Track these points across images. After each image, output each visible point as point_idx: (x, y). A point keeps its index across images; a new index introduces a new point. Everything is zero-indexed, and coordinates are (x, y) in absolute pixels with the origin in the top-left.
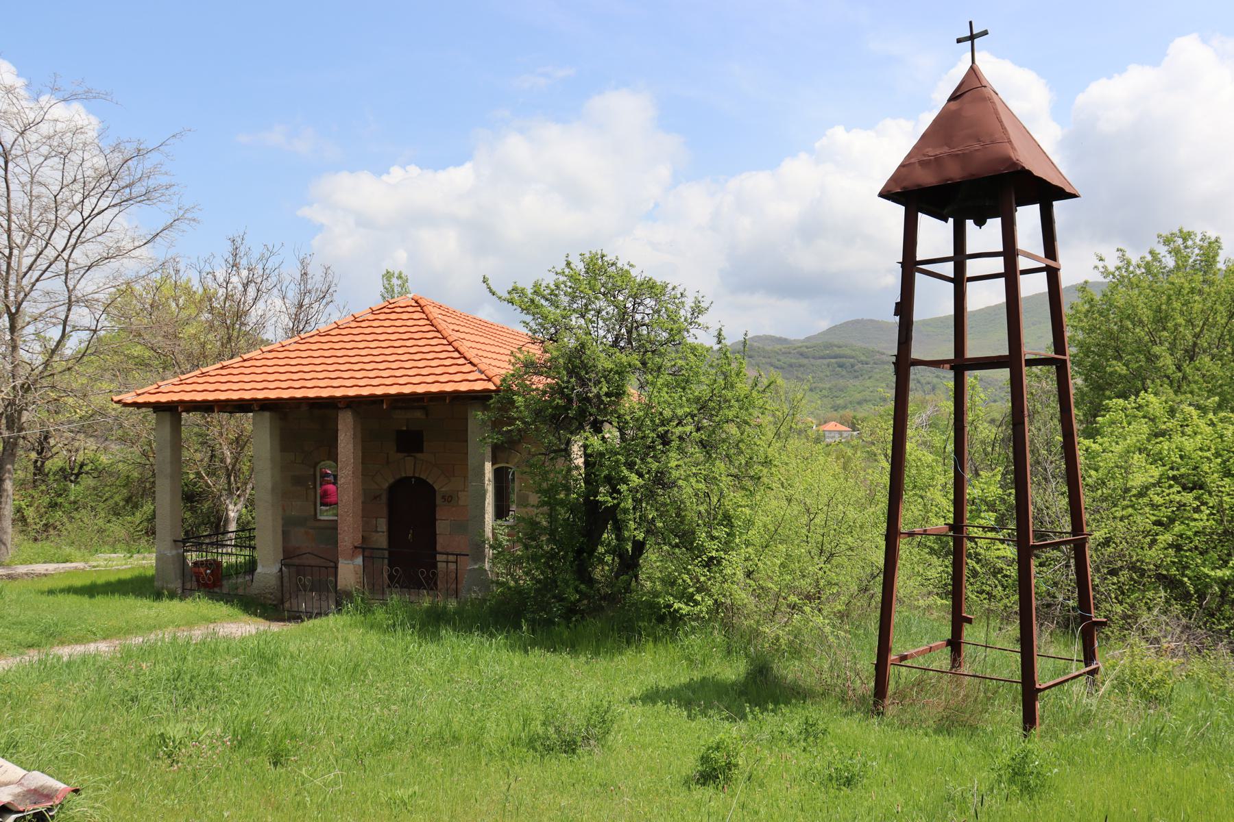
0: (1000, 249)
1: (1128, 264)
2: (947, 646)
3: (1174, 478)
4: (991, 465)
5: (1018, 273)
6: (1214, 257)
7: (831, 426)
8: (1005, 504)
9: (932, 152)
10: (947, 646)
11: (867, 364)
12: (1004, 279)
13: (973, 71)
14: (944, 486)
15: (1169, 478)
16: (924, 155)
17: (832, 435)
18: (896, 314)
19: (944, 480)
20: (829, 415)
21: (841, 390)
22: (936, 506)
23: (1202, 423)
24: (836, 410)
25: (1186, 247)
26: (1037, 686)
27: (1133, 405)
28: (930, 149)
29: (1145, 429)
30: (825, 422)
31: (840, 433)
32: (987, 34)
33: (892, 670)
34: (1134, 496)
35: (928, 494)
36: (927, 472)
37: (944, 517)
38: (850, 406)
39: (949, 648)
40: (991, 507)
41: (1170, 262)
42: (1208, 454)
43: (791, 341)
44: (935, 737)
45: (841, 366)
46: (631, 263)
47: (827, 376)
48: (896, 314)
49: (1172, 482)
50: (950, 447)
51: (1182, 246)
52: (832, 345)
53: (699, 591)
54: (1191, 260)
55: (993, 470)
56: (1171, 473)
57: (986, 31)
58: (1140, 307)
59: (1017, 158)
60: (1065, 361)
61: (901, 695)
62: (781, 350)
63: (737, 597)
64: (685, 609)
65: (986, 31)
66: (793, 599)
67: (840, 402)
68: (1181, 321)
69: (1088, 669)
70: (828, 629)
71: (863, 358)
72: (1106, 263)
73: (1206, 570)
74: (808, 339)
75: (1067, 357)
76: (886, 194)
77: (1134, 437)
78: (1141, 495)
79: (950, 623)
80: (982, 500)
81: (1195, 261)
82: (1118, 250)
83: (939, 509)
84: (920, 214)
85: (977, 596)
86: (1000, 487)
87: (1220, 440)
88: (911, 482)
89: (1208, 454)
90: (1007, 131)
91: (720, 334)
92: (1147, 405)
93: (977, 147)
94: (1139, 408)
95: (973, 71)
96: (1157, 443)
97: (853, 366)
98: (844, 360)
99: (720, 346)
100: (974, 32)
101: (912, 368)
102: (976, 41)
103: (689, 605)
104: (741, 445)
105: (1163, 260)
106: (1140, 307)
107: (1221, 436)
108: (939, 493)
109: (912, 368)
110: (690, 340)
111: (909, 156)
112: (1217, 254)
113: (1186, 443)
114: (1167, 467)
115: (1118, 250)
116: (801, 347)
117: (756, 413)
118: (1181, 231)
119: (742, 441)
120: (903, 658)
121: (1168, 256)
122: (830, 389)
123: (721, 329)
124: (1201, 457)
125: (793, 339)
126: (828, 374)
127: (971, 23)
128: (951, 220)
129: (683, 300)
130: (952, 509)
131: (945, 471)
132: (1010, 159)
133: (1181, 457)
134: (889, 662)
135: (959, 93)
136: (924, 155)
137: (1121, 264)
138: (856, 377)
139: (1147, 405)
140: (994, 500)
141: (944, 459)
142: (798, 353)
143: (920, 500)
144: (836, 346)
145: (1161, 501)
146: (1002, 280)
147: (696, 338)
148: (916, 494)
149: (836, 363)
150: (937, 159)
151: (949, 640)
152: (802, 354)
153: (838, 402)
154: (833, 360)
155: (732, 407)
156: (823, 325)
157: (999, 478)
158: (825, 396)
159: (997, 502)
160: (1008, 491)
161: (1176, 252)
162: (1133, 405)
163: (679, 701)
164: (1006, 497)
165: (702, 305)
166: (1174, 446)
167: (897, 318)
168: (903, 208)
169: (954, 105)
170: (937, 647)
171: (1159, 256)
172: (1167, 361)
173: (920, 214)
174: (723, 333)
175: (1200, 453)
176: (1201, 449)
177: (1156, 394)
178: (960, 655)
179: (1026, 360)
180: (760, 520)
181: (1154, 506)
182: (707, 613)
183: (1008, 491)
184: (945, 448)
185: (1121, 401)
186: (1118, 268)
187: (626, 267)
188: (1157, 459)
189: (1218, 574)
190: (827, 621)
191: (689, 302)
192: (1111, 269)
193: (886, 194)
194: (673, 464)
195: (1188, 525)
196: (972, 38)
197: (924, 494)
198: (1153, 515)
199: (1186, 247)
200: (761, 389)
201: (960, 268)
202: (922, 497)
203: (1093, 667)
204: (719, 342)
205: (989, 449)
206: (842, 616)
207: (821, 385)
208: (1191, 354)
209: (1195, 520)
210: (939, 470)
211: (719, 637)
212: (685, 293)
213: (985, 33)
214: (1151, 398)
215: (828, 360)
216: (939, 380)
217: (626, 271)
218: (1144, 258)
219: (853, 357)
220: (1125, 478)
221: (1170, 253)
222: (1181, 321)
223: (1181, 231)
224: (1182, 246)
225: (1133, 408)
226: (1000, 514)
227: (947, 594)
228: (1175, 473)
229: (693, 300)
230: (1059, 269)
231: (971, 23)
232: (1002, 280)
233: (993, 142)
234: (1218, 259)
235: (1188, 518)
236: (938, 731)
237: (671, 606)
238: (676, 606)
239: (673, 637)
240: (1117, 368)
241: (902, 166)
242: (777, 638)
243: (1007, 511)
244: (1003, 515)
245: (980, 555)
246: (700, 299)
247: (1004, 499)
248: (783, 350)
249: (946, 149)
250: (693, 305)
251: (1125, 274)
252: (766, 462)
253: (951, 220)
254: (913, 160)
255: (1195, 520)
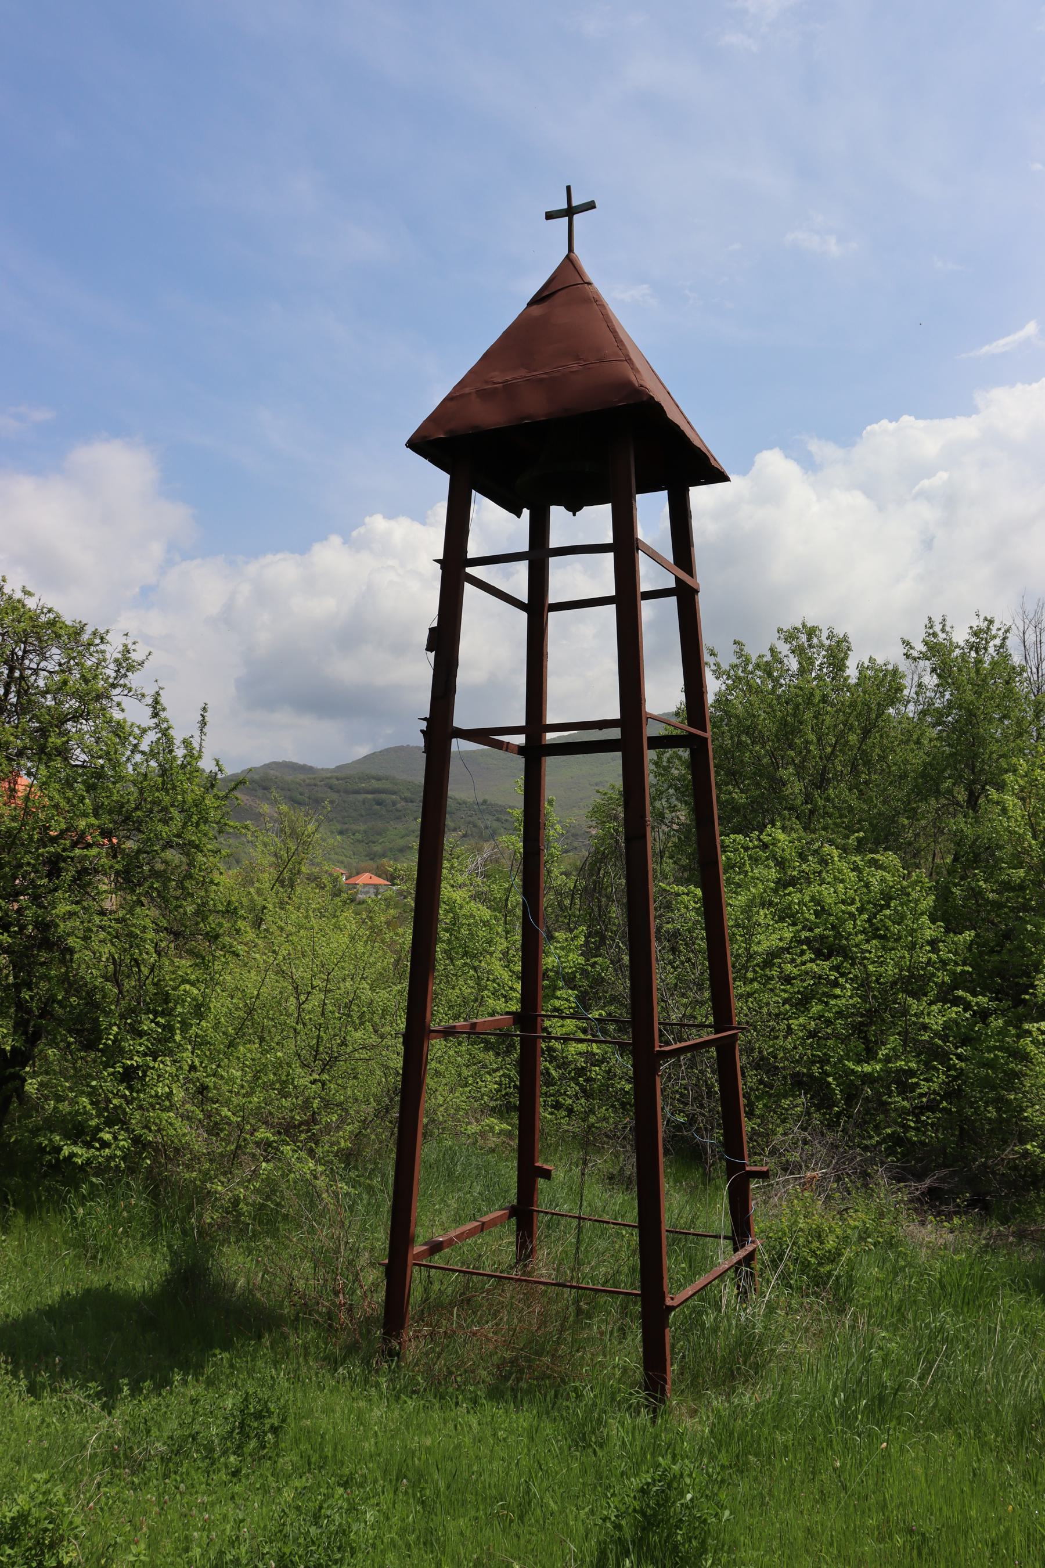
0: (609, 538)
1: (747, 661)
2: (510, 1217)
3: (807, 941)
4: (568, 924)
5: (639, 596)
6: (843, 660)
7: (365, 878)
8: (587, 978)
9: (499, 377)
10: (510, 1217)
11: (412, 802)
12: (614, 606)
13: (570, 261)
14: (505, 953)
15: (801, 942)
16: (487, 382)
17: (366, 889)
18: (429, 648)
19: (505, 944)
20: (363, 864)
21: (379, 834)
22: (494, 981)
23: (844, 866)
24: (372, 859)
25: (811, 646)
26: (669, 1302)
27: (756, 843)
28: (496, 373)
29: (773, 873)
30: (358, 874)
31: (376, 887)
32: (594, 207)
33: (416, 1276)
34: (757, 965)
35: (483, 964)
36: (482, 933)
37: (505, 997)
38: (389, 853)
39: (514, 1220)
40: (570, 982)
41: (793, 664)
42: (852, 909)
43: (318, 770)
44: (489, 1408)
45: (379, 803)
46: (28, 589)
47: (362, 816)
48: (429, 648)
49: (805, 947)
50: (517, 898)
51: (806, 644)
52: (370, 777)
53: (109, 1123)
54: (817, 663)
55: (571, 931)
56: (804, 934)
57: (593, 202)
58: (761, 718)
59: (642, 382)
60: (706, 739)
61: (434, 1307)
62: (304, 781)
63: (172, 1132)
64: (81, 1153)
65: (593, 202)
66: (264, 1133)
67: (377, 848)
68: (812, 737)
69: (742, 1254)
70: (321, 1183)
71: (408, 795)
72: (719, 659)
73: (850, 1065)
74: (339, 768)
75: (708, 735)
76: (420, 444)
77: (760, 885)
78: (768, 964)
79: (515, 1155)
80: (557, 973)
81: (822, 664)
82: (735, 643)
83: (499, 985)
84: (473, 492)
85: (551, 1113)
86: (581, 955)
87: (865, 890)
88: (460, 946)
89: (852, 909)
90: (623, 345)
91: (156, 702)
92: (773, 844)
93: (575, 367)
94: (765, 846)
95: (570, 261)
96: (785, 895)
97: (394, 803)
98: (383, 796)
99: (156, 720)
100: (575, 203)
101: (454, 740)
102: (576, 218)
103: (93, 1147)
104: (187, 884)
105: (785, 660)
106: (761, 718)
107: (867, 885)
108: (497, 963)
109: (454, 740)
110: (117, 715)
111: (461, 384)
112: (846, 657)
113: (825, 893)
114: (799, 927)
115: (735, 643)
116: (329, 778)
117: (211, 830)
118: (804, 625)
119: (189, 876)
120: (435, 1248)
121: (791, 656)
122: (365, 832)
123: (158, 694)
124: (843, 912)
125: (320, 767)
126: (364, 813)
127: (569, 188)
128: (526, 513)
129: (102, 647)
130: (518, 986)
131: (507, 932)
132: (629, 383)
133: (817, 914)
134: (410, 1261)
135: (546, 293)
136: (487, 382)
137: (737, 661)
138: (398, 818)
139: (773, 844)
140: (574, 973)
141: (506, 916)
142: (326, 785)
143: (472, 972)
144: (374, 778)
145: (796, 971)
146: (612, 608)
147: (123, 710)
148: (465, 964)
149: (374, 799)
150: (508, 388)
151: (513, 1207)
152: (331, 788)
153: (375, 849)
154: (370, 796)
155: (171, 819)
156: (362, 751)
157: (582, 940)
158: (359, 841)
159: (577, 975)
160: (593, 960)
161: (799, 651)
162: (756, 843)
163: (13, 1356)
164: (590, 968)
165: (133, 656)
166: (807, 898)
167: (432, 655)
168: (448, 476)
169: (537, 310)
170: (494, 1222)
171: (781, 656)
172: (795, 788)
173: (473, 492)
174: (163, 700)
175: (843, 907)
176: (843, 902)
177: (784, 828)
178: (531, 1235)
179: (649, 739)
180: (219, 1004)
181: (788, 980)
182: (124, 1158)
183: (593, 960)
184: (507, 900)
185: (740, 837)
186: (734, 667)
187: (18, 595)
188: (786, 915)
189: (865, 1070)
190: (320, 1168)
191: (112, 650)
192: (725, 667)
193: (420, 444)
194: (63, 908)
195: (827, 1004)
196: (570, 212)
197: (476, 964)
198: (784, 991)
199: (811, 646)
200: (221, 794)
201: (538, 581)
202: (475, 969)
203: (749, 1248)
204: (155, 715)
205: (567, 902)
206: (349, 1157)
207: (355, 827)
208: (821, 782)
209: (836, 997)
210: (500, 930)
211: (138, 1202)
212: (108, 638)
213: (591, 206)
214: (781, 836)
215: (364, 796)
216: (500, 824)
217: (19, 601)
218: (763, 656)
219: (394, 793)
220: (748, 941)
221: (793, 652)
222: (812, 737)
223: (804, 625)
224: (806, 644)
225: (755, 847)
226: (580, 992)
227: (509, 1108)
228: (808, 934)
229: (121, 648)
230: (697, 592)
231: (569, 188)
232: (612, 608)
233: (601, 361)
234: (848, 663)
235: (824, 994)
236: (495, 1394)
237: (59, 1149)
238: (66, 1151)
239: (58, 1202)
240: (734, 795)
241: (449, 399)
242: (236, 1202)
243: (591, 987)
244: (586, 993)
245: (555, 1050)
246: (131, 647)
247: (586, 970)
248: (308, 781)
249: (523, 372)
250: (120, 656)
251: (742, 675)
252: (227, 911)
253: (526, 513)
254: (467, 390)
255: (836, 997)
